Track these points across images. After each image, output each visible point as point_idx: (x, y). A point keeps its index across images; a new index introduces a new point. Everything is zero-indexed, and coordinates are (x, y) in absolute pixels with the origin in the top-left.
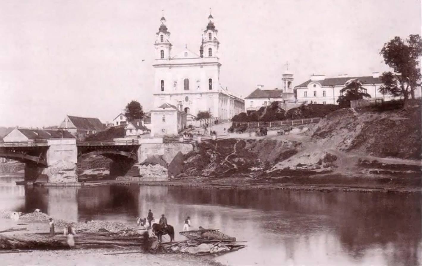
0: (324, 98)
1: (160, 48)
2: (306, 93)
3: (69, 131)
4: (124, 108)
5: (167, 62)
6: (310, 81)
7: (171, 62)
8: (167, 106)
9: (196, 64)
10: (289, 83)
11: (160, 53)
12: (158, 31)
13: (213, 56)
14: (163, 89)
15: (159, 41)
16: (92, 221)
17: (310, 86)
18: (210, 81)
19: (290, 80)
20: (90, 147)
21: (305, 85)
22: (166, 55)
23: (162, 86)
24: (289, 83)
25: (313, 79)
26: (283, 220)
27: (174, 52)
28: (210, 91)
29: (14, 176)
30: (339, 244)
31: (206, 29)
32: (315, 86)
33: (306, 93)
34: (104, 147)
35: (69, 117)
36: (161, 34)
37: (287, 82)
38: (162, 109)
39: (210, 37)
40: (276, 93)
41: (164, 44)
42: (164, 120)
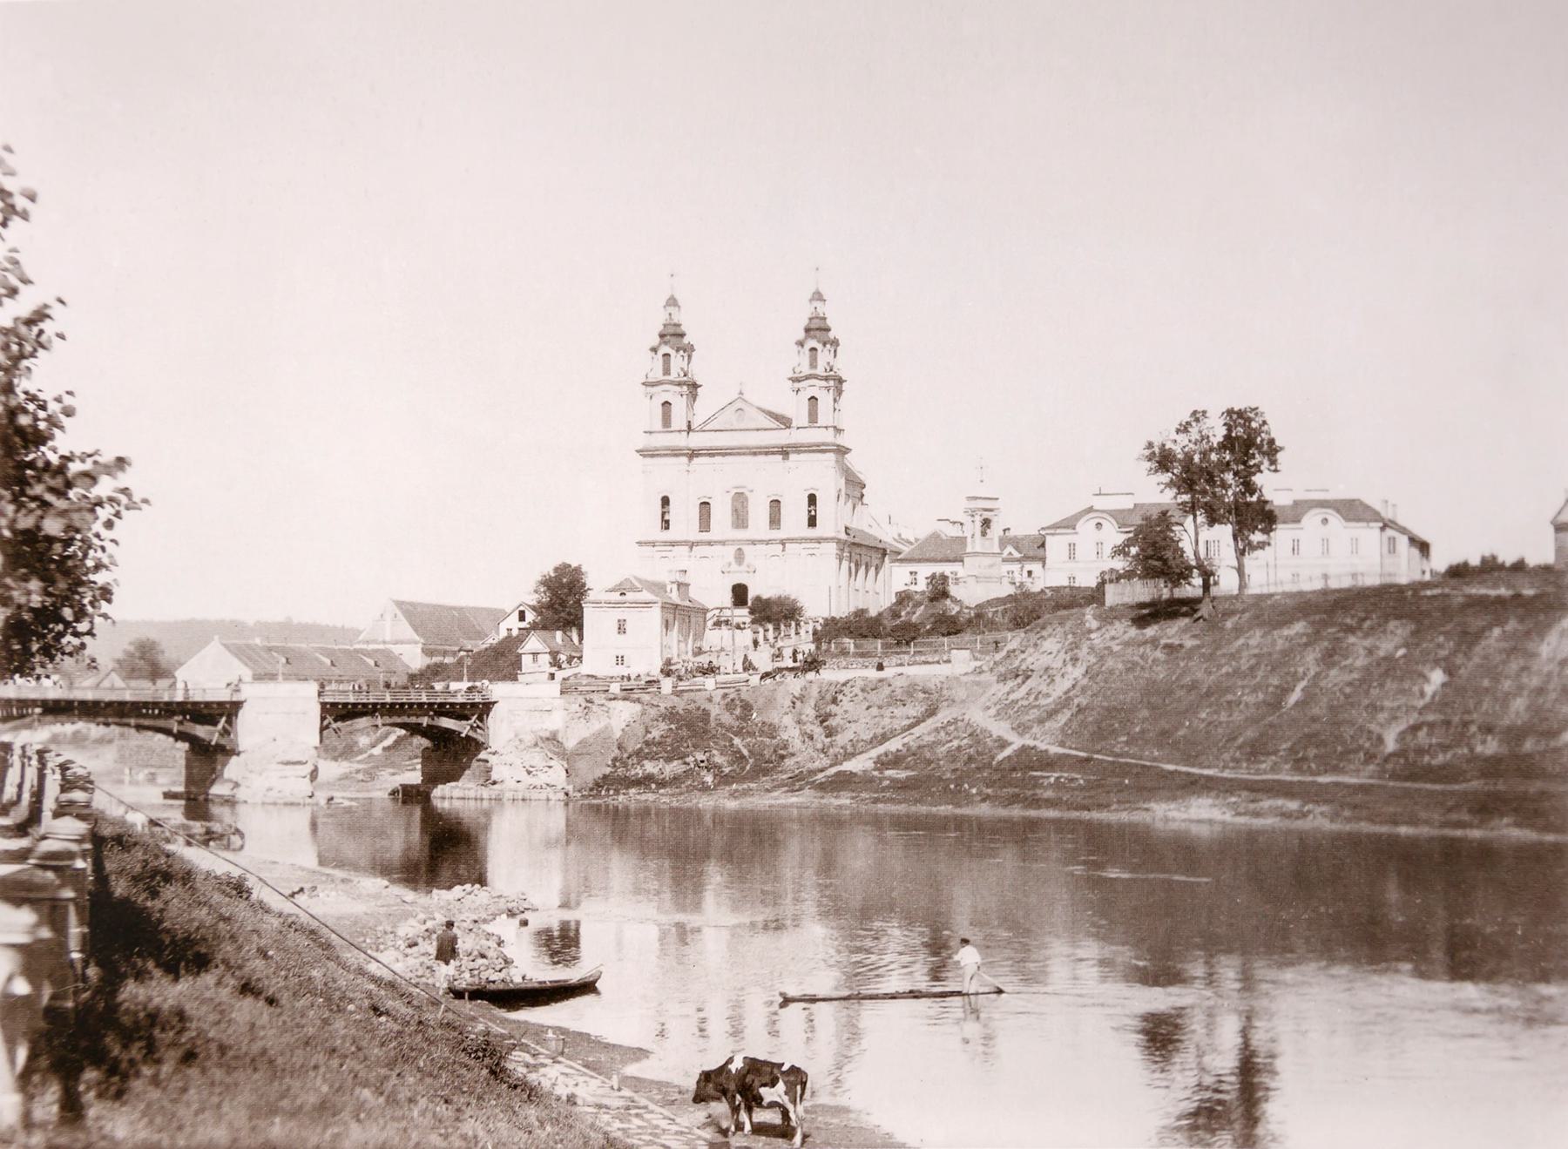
0: (1072, 565)
1: (663, 394)
2: (1072, 546)
3: (396, 649)
4: (532, 585)
5: (681, 441)
6: (1090, 510)
7: (696, 440)
8: (634, 589)
9: (767, 451)
10: (986, 523)
11: (659, 410)
12: (657, 340)
13: (822, 421)
14: (666, 524)
15: (658, 374)
16: (1177, 1060)
17: (1086, 527)
18: (812, 499)
19: (987, 515)
20: (355, 705)
21: (1069, 524)
22: (678, 421)
23: (663, 514)
24: (986, 523)
25: (1099, 503)
26: (844, 868)
27: (705, 407)
28: (812, 533)
29: (901, 809)
30: (1385, 980)
31: (801, 335)
32: (1099, 525)
33: (1072, 546)
34: (392, 705)
35: (400, 604)
36: (665, 349)
37: (978, 519)
38: (616, 596)
39: (813, 364)
40: (954, 551)
41: (672, 383)
42: (621, 629)
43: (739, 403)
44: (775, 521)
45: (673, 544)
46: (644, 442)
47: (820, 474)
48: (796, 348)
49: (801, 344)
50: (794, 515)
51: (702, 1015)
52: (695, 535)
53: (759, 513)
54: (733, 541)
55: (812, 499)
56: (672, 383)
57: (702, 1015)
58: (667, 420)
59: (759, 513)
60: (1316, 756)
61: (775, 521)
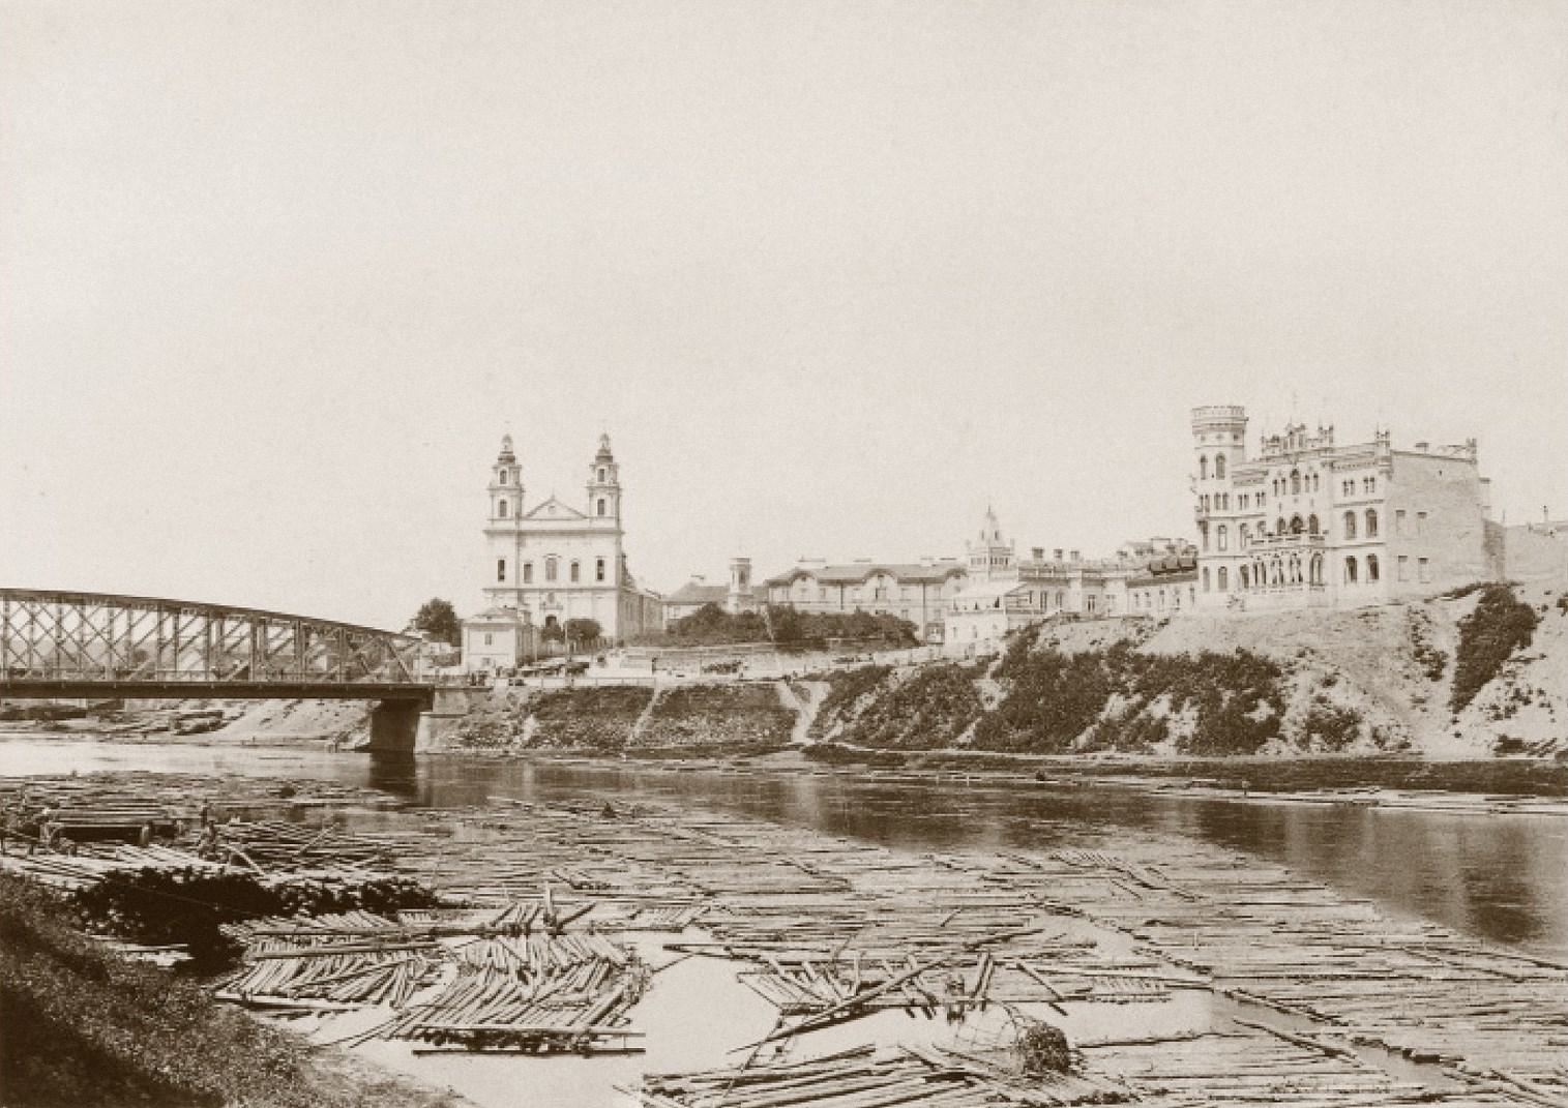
15: (597, 483)
43: (550, 504)
44: (575, 576)
45: (581, 590)
46: (488, 525)
47: (605, 548)
48: (590, 470)
49: (495, 468)
50: (588, 575)
51: (1552, 716)
52: (546, 584)
53: (564, 572)
54: (547, 590)
55: (600, 564)
56: (506, 489)
57: (1552, 716)
58: (503, 512)
59: (564, 572)
60: (1219, 682)
61: (575, 576)
